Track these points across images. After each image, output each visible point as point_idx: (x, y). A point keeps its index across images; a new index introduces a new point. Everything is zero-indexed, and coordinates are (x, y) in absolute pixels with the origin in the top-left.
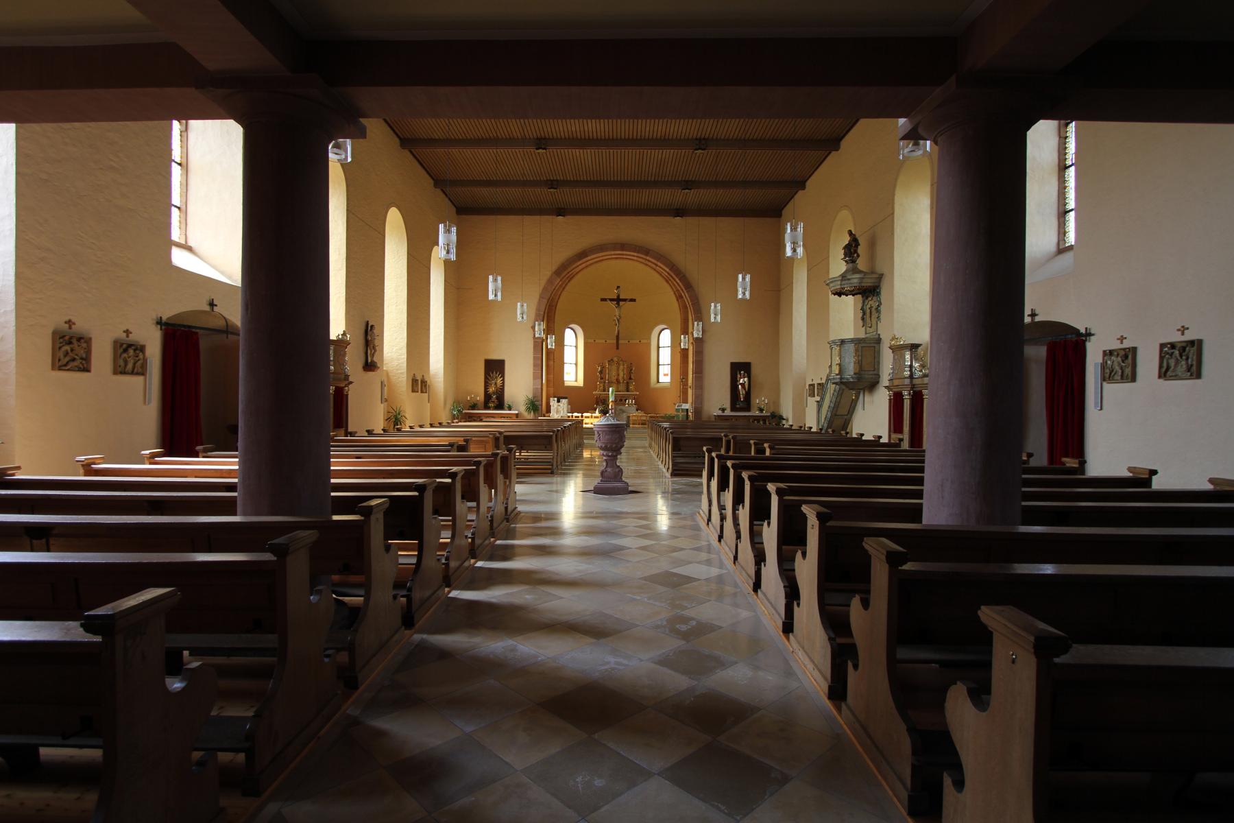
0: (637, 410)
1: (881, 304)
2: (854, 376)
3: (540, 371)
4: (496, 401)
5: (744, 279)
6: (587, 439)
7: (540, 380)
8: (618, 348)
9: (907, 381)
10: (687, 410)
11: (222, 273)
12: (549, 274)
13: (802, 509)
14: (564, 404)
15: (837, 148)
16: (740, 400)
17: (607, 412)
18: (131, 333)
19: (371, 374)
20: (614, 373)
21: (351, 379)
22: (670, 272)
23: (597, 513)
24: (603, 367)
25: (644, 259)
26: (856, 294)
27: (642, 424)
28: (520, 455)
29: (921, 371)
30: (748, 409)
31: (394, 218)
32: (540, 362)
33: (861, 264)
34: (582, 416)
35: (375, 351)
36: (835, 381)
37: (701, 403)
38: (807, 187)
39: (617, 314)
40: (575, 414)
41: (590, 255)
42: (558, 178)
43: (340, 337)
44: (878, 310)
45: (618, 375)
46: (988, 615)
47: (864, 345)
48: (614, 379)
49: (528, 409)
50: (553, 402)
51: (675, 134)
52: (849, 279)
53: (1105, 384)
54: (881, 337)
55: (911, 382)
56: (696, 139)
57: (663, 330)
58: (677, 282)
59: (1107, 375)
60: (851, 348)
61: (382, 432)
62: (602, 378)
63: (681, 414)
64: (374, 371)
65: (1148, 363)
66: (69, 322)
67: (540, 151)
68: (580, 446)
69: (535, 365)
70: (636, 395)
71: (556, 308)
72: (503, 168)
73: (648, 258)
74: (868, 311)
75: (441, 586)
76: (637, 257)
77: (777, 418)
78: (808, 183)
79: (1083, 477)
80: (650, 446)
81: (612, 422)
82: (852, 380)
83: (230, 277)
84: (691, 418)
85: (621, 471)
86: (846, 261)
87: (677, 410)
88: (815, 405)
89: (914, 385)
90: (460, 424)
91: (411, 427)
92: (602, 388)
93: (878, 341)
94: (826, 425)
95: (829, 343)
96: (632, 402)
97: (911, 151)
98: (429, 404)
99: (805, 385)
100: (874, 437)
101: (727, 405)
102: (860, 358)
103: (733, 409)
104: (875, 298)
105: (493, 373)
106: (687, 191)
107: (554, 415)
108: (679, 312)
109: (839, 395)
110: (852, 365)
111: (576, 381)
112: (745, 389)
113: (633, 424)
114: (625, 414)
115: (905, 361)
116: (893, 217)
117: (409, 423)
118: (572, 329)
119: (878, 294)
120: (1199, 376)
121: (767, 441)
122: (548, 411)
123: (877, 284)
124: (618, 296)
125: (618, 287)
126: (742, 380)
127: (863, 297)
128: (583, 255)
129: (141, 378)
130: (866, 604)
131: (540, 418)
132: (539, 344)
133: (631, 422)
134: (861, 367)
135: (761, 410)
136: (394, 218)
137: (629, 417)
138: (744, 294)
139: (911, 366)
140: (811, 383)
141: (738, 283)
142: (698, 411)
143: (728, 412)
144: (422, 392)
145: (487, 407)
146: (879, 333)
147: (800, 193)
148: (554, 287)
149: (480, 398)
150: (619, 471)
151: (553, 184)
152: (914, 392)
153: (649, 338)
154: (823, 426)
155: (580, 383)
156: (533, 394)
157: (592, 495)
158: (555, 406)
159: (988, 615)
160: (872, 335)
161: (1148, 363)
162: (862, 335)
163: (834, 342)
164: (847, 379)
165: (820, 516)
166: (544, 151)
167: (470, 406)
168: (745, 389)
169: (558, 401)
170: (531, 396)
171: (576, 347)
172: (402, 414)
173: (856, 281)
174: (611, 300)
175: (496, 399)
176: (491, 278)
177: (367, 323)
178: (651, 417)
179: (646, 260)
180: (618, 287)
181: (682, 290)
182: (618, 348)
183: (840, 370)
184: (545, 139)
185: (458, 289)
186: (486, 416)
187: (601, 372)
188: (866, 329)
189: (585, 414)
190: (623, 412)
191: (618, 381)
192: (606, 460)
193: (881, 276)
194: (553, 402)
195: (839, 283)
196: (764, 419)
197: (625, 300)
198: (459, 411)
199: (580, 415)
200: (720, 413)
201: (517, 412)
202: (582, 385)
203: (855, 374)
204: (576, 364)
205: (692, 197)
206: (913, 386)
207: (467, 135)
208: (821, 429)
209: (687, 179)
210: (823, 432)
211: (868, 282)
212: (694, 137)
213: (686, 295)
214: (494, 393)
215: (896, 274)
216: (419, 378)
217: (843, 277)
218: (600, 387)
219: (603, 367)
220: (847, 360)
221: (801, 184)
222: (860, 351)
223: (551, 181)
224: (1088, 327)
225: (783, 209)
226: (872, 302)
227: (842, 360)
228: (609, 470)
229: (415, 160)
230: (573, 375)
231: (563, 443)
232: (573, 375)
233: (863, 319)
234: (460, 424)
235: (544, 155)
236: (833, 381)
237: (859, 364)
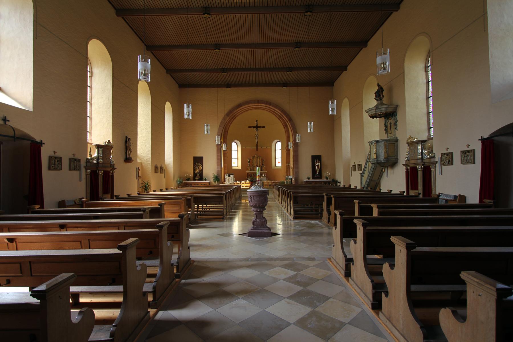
0: (267, 179)
1: (397, 121)
2: (384, 159)
3: (220, 162)
4: (199, 176)
5: (310, 124)
6: (243, 194)
7: (220, 166)
8: (257, 150)
9: (420, 161)
10: (291, 179)
11: (20, 103)
12: (223, 115)
15: (366, 46)
16: (316, 174)
17: (255, 182)
18: (56, 152)
19: (129, 164)
20: (255, 162)
21: (115, 166)
22: (281, 113)
23: (252, 260)
24: (250, 160)
25: (268, 107)
26: (382, 117)
27: (269, 186)
28: (206, 206)
29: (429, 155)
30: (321, 178)
31: (168, 106)
32: (220, 157)
33: (385, 100)
34: (241, 183)
35: (131, 152)
36: (374, 162)
37: (298, 175)
38: (335, 85)
39: (256, 134)
40: (238, 182)
41: (243, 106)
42: (227, 67)
43: (106, 143)
44: (395, 124)
45: (257, 163)
47: (389, 143)
49: (215, 180)
50: (227, 177)
51: (284, 41)
52: (380, 108)
53: (443, 167)
54: (398, 138)
55: (422, 161)
56: (295, 43)
57: (277, 142)
58: (285, 118)
59: (443, 163)
60: (382, 144)
61: (127, 196)
62: (250, 165)
63: (288, 181)
64: (130, 162)
65: (457, 158)
66: (74, 155)
67: (217, 50)
68: (240, 198)
69: (217, 159)
70: (266, 172)
71: (227, 133)
72: (199, 62)
73: (271, 107)
74: (389, 125)
76: (265, 106)
77: (335, 182)
78: (348, 67)
79: (465, 204)
80: (275, 197)
81: (259, 189)
82: (383, 162)
83: (25, 106)
84: (294, 183)
85: (266, 221)
86: (377, 100)
87: (287, 179)
88: (359, 175)
89: (425, 163)
90: (179, 189)
91: (154, 191)
92: (250, 169)
93: (397, 140)
94: (366, 185)
95: (369, 142)
96: (264, 175)
98: (165, 179)
99: (349, 165)
100: (354, 187)
101: (311, 176)
102: (387, 149)
103: (313, 178)
104: (393, 118)
105: (197, 163)
106: (289, 72)
107: (227, 183)
108: (285, 132)
109: (374, 170)
110: (383, 153)
111: (238, 166)
112: (319, 168)
113: (265, 186)
115: (418, 150)
116: (362, 102)
117: (153, 189)
118: (235, 142)
119: (396, 116)
120: (452, 164)
121: (356, 198)
122: (225, 181)
123: (394, 111)
124: (257, 125)
125: (257, 121)
126: (317, 164)
127: (385, 119)
128: (239, 106)
129: (78, 172)
131: (220, 184)
132: (219, 146)
133: (264, 185)
134: (388, 154)
135: (327, 178)
136: (168, 106)
137: (263, 183)
138: (333, 111)
139: (422, 152)
140: (354, 164)
141: (329, 105)
142: (296, 179)
143: (311, 180)
144: (161, 173)
145: (195, 180)
146: (396, 136)
147: (345, 72)
148: (226, 122)
149: (192, 175)
150: (264, 221)
151: (224, 70)
152: (424, 167)
153: (271, 146)
154: (365, 186)
155: (240, 167)
156: (217, 173)
157: (247, 238)
160: (391, 136)
161: (457, 158)
162: (385, 137)
163: (372, 142)
164: (380, 161)
166: (219, 50)
167: (186, 179)
168: (319, 168)
169: (229, 176)
170: (216, 174)
171: (237, 151)
172: (149, 184)
173: (384, 109)
174: (253, 127)
175: (199, 176)
176: (185, 105)
177: (127, 137)
178: (273, 182)
179: (270, 108)
180: (257, 121)
181: (287, 122)
182: (257, 150)
183: (376, 157)
184: (219, 44)
185: (180, 123)
186: (201, 184)
187: (249, 162)
188: (388, 135)
189: (242, 182)
192: (255, 214)
193: (397, 106)
194: (227, 177)
195: (374, 110)
196: (329, 182)
197: (260, 127)
198: (180, 182)
199: (240, 182)
200: (307, 180)
201: (209, 182)
202: (241, 168)
203: (385, 158)
204: (238, 159)
205: (292, 76)
206: (424, 164)
207: (180, 43)
208: (363, 188)
209: (289, 66)
210: (365, 189)
211: (390, 110)
212: (294, 41)
213: (289, 124)
214: (198, 173)
215: (407, 104)
216: (159, 166)
217: (376, 107)
218: (249, 169)
219: (250, 160)
220: (380, 151)
221: (345, 68)
222: (387, 145)
223: (223, 69)
224: (483, 136)
225: (334, 82)
226: (391, 121)
227: (377, 151)
228: (258, 220)
229: (155, 58)
230: (236, 163)
231: (230, 199)
232: (236, 163)
233: (385, 130)
234: (179, 189)
235: (219, 52)
236: (372, 163)
237: (387, 153)
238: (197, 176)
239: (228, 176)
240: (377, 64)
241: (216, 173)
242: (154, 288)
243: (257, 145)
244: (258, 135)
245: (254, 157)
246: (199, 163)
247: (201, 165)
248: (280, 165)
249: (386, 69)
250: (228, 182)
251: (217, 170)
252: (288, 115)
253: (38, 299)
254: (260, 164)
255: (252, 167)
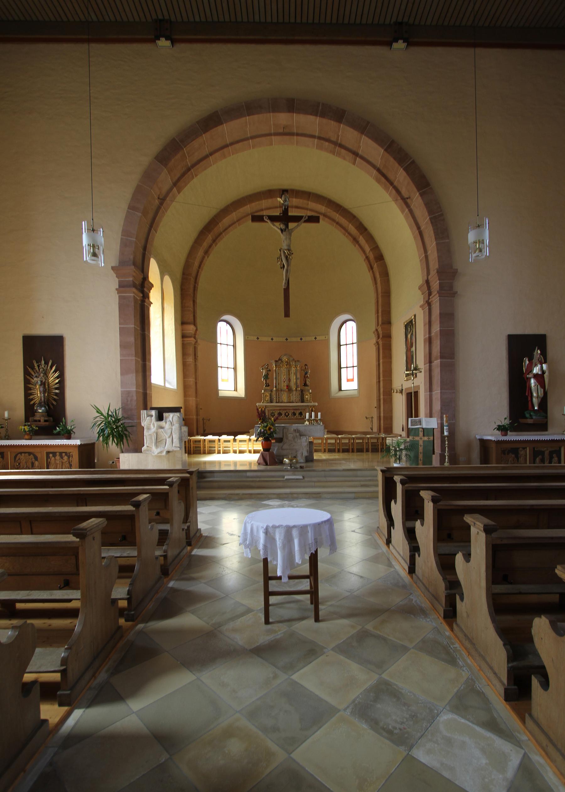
13: (556, 571)
14: (172, 424)
20: (283, 377)
30: (543, 427)
45: (289, 380)
46: (468, 519)
48: (284, 386)
57: (345, 322)
62: (267, 385)
70: (314, 406)
75: (185, 546)
92: (268, 398)
96: (316, 416)
97: (477, 256)
105: (39, 361)
111: (236, 390)
114: (304, 439)
118: (228, 323)
124: (286, 211)
130: (395, 502)
153: (327, 333)
155: (241, 392)
158: (153, 429)
159: (468, 519)
165: (434, 500)
169: (160, 418)
171: (234, 346)
174: (273, 219)
187: (266, 377)
189: (239, 437)
190: (301, 435)
191: (289, 387)
204: (235, 369)
209: (400, 20)
238: (33, 415)
239: (154, 418)
240: (469, 243)
241: (119, 405)
242: (129, 593)
243: (287, 291)
244: (289, 250)
245: (278, 361)
246: (46, 363)
247: (55, 371)
248: (354, 385)
249: (483, 252)
250: (157, 446)
251: (123, 393)
252: (413, 162)
253: (77, 538)
254: (298, 381)
255: (274, 393)
